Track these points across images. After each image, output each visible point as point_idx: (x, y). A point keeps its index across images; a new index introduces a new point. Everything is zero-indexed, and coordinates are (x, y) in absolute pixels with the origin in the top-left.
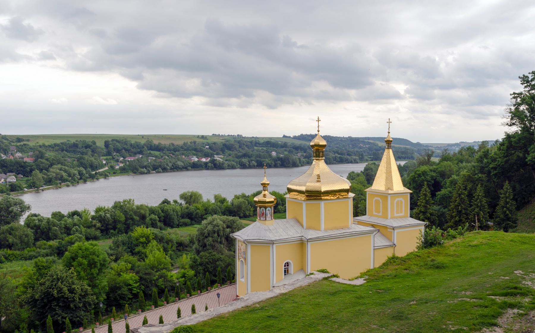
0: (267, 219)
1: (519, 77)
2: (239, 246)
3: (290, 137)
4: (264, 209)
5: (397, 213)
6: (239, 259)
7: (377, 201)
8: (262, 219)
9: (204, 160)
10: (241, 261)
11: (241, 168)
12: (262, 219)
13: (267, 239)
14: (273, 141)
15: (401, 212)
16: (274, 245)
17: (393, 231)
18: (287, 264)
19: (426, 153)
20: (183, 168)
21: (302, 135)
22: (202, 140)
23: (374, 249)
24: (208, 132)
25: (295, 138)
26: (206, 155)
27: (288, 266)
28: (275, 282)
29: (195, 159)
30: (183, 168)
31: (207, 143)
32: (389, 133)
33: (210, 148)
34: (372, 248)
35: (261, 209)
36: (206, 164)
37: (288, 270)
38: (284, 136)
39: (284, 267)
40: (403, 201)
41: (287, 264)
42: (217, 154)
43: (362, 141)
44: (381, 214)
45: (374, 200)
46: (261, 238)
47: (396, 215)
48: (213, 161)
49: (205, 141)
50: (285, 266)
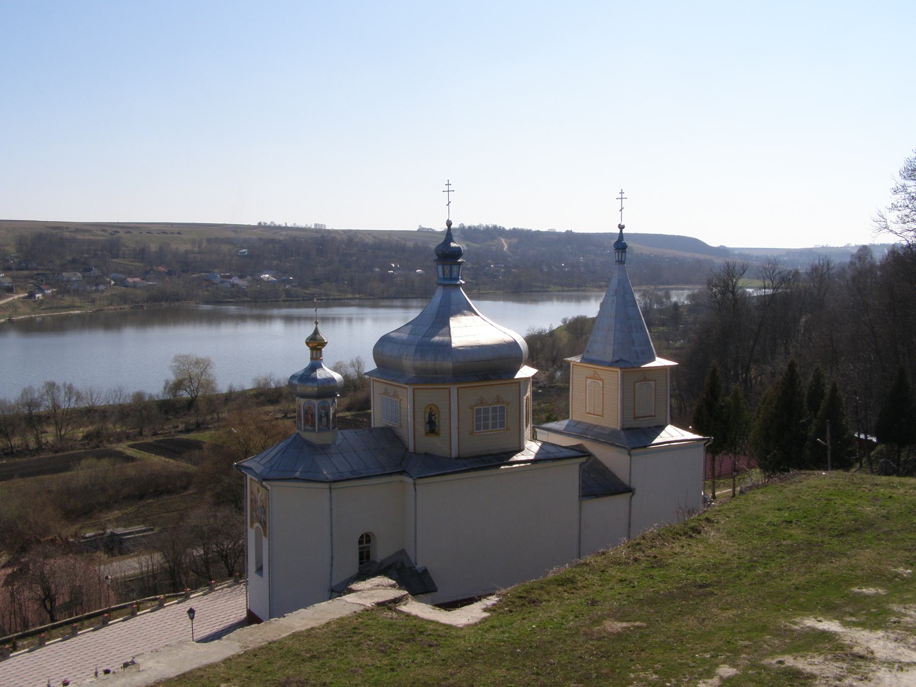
2: (252, 493)
10: (257, 528)
14: (746, 252)
16: (454, 454)
18: (366, 539)
19: (723, 276)
27: (368, 541)
50: (360, 542)
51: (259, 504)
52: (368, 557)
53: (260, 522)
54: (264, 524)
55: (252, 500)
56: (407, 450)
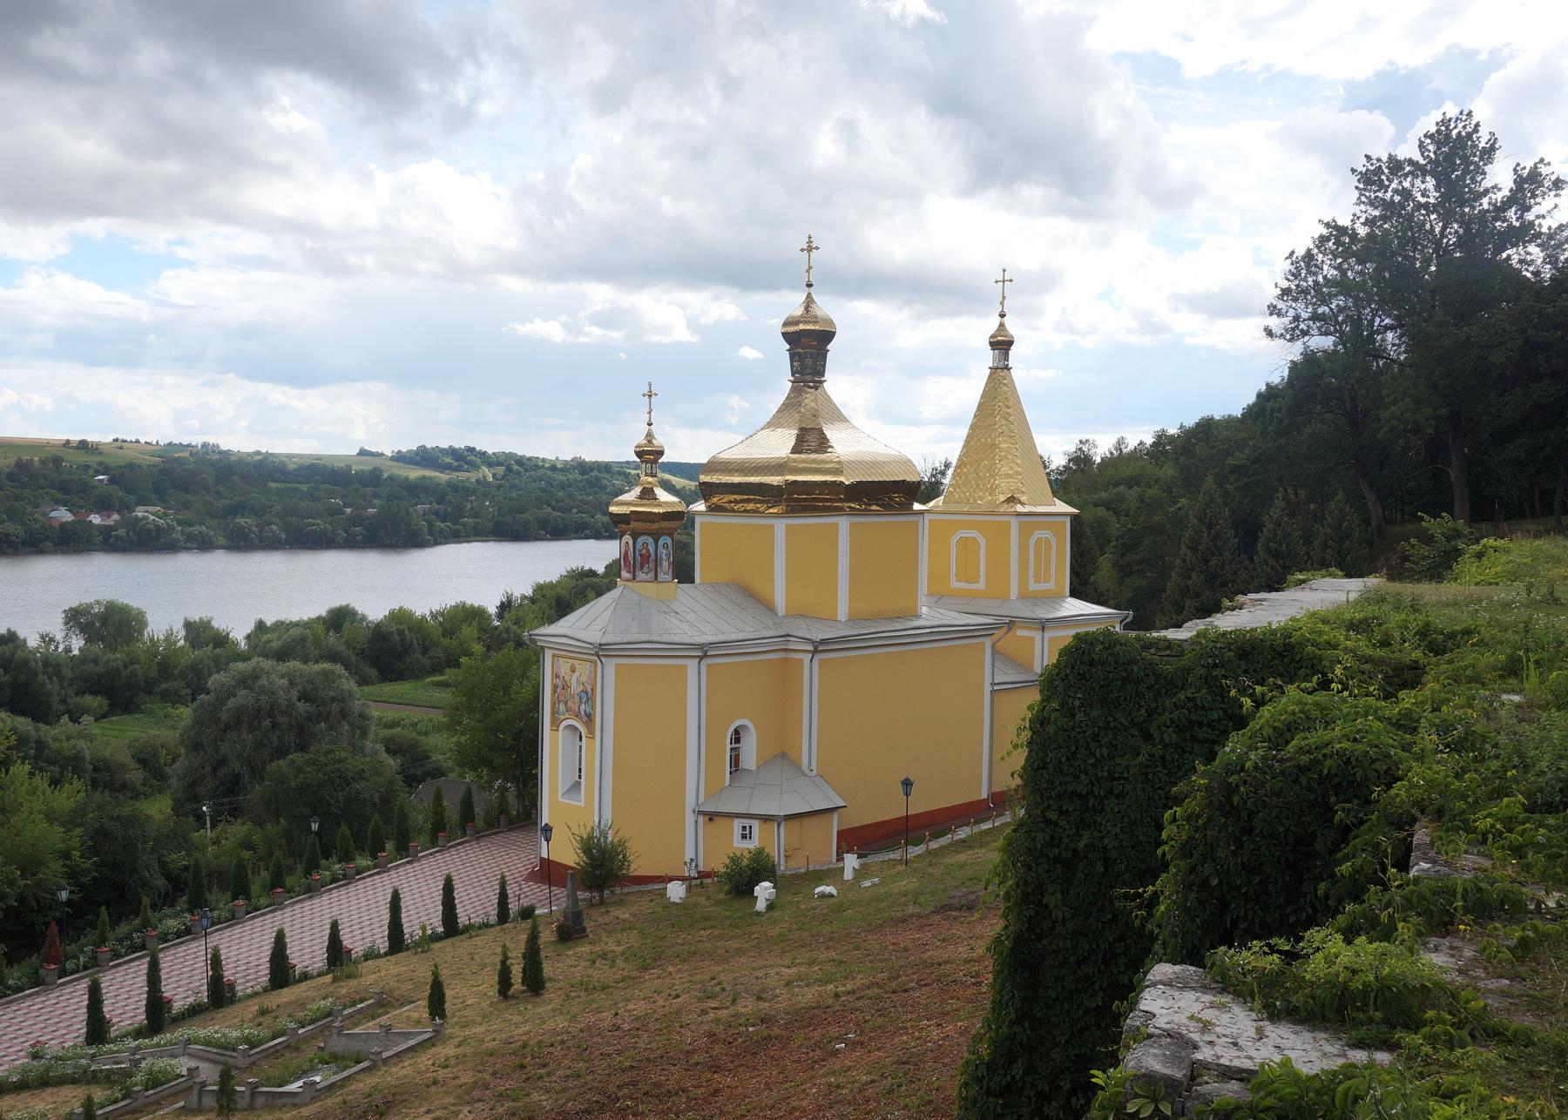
0: (661, 576)
1: (1353, 171)
3: (381, 455)
4: (650, 540)
5: (1037, 581)
6: (555, 722)
7: (967, 546)
8: (641, 575)
9: (96, 519)
10: (573, 728)
11: (228, 548)
12: (641, 575)
13: (677, 639)
15: (1047, 580)
17: (1037, 635)
20: (24, 543)
21: (422, 449)
22: (84, 458)
23: (993, 692)
24: (100, 435)
25: (400, 458)
26: (104, 506)
27: (738, 740)
28: (701, 800)
29: (63, 515)
30: (24, 543)
31: (100, 464)
32: (1002, 316)
33: (112, 481)
34: (988, 689)
35: (640, 540)
36: (106, 532)
37: (737, 756)
38: (363, 452)
39: (728, 747)
40: (1054, 542)
41: (737, 736)
42: (144, 502)
43: (619, 473)
44: (981, 585)
45: (954, 541)
46: (656, 638)
47: (1033, 586)
48: (133, 525)
49: (93, 460)
51: (575, 688)
52: (737, 765)
53: (578, 715)
54: (589, 719)
55: (555, 687)
56: (770, 608)
